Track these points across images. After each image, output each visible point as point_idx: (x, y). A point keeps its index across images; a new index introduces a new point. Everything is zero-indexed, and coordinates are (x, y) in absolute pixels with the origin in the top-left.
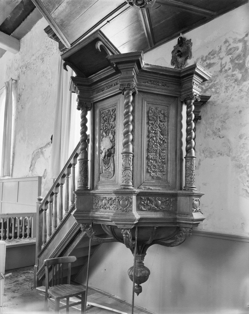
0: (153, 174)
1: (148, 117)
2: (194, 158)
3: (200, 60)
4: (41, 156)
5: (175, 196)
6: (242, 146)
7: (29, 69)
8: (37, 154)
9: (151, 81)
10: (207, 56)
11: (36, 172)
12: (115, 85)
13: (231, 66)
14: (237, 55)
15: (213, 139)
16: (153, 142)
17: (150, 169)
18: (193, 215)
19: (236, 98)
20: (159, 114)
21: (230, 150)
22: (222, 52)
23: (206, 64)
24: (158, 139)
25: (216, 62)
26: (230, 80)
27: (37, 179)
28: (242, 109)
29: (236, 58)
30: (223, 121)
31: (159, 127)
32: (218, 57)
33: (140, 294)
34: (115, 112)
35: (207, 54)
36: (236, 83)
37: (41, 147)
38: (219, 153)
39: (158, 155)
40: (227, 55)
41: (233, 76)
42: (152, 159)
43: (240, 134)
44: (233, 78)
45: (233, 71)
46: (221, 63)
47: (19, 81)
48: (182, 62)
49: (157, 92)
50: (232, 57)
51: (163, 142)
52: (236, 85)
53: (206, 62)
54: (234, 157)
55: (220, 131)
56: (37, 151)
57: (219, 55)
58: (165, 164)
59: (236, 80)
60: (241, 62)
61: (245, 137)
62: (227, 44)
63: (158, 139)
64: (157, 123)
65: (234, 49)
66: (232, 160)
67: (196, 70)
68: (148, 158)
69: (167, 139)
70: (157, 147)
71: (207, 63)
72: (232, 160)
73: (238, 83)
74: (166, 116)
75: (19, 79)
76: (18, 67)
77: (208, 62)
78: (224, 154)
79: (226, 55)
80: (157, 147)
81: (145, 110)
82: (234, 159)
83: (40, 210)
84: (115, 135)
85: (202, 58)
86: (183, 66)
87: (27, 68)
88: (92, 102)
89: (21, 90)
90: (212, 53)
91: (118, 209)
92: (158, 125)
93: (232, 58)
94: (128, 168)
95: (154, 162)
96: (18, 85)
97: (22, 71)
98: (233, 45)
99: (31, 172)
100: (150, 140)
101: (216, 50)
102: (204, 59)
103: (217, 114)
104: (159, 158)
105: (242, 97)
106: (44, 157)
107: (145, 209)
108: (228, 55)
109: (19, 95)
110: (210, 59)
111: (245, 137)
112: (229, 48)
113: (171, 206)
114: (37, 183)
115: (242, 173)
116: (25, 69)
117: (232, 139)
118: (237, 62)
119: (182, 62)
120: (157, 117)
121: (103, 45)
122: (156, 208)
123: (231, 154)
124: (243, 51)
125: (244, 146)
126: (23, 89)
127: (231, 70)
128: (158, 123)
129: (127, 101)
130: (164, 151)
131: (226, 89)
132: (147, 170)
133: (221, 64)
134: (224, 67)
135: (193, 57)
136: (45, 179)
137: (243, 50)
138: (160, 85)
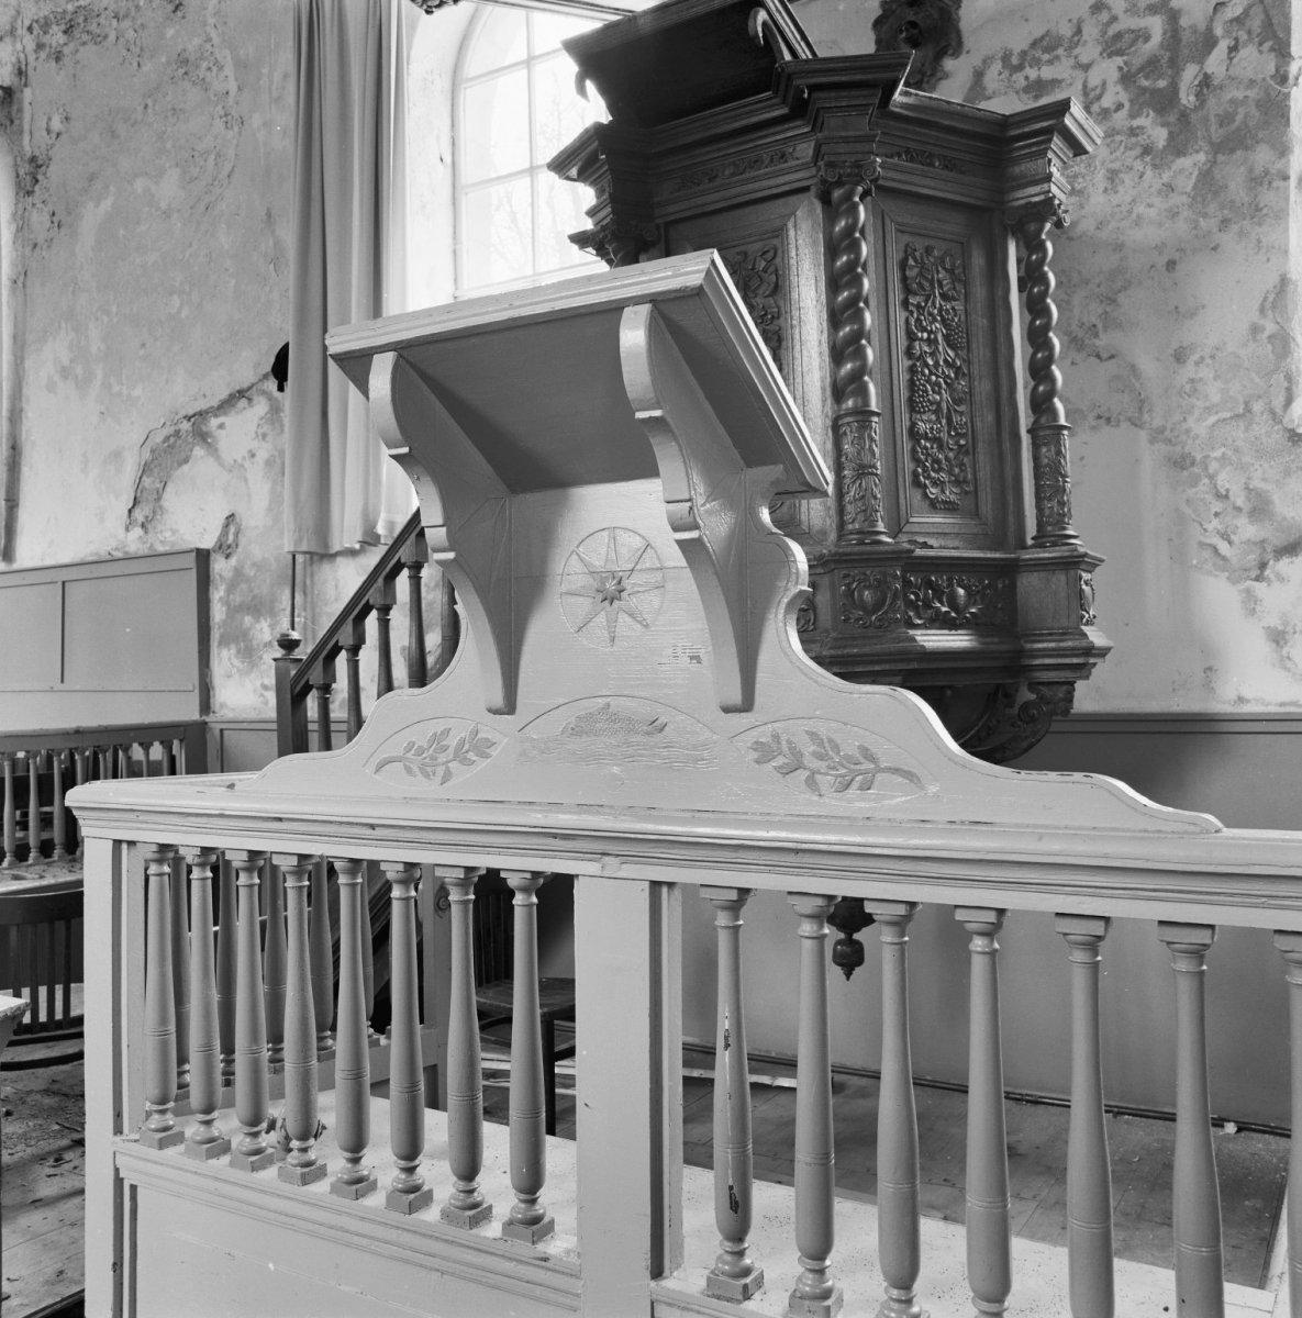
0: (933, 491)
1: (904, 279)
2: (1066, 432)
3: (997, 66)
4: (199, 451)
5: (1010, 570)
6: (1188, 388)
7: (85, 37)
8: (171, 447)
9: (908, 151)
10: (1024, 53)
11: (174, 532)
12: (772, 160)
13: (1124, 97)
14: (1145, 58)
15: (1073, 363)
16: (927, 371)
17: (924, 471)
18: (1086, 635)
19: (1152, 212)
20: (938, 272)
21: (1142, 404)
22: (1086, 41)
23: (1023, 83)
24: (941, 363)
25: (1065, 75)
26: (1122, 149)
27: (191, 561)
28: (1177, 256)
29: (1141, 69)
30: (1109, 298)
31: (941, 316)
32: (1072, 61)
33: (858, 971)
34: (778, 260)
35: (1024, 45)
36: (1148, 159)
37: (191, 412)
38: (1099, 417)
39: (944, 421)
40: (1105, 55)
41: (1133, 132)
42: (927, 439)
43: (1175, 345)
44: (1133, 140)
45: (1133, 116)
46: (1085, 81)
47: (27, 92)
48: (923, 65)
49: (931, 192)
50: (1126, 63)
51: (956, 374)
52: (1149, 168)
53: (1024, 73)
54: (1161, 430)
55: (1096, 335)
56: (169, 430)
57: (1076, 51)
58: (967, 453)
59: (1147, 150)
60: (1162, 84)
61: (1196, 357)
62: (1104, 17)
63: (941, 363)
64: (934, 303)
65: (1132, 36)
66: (1152, 441)
67: (1068, 121)
68: (913, 433)
69: (968, 362)
70: (940, 393)
71: (1027, 78)
72: (1152, 441)
73: (1158, 161)
74: (960, 278)
75: (26, 85)
76: (15, 19)
77: (1033, 73)
78: (1119, 421)
79: (1101, 54)
80: (940, 393)
81: (895, 256)
82: (1157, 435)
83: (298, 688)
84: (779, 347)
85: (1006, 58)
86: (928, 82)
87: (77, 33)
88: (659, 221)
89: (42, 138)
90: (1045, 43)
91: (849, 618)
92: (936, 311)
93: (1126, 69)
94: (871, 467)
95: (932, 448)
96: (20, 110)
97: (40, 46)
98: (1127, 22)
99: (138, 531)
100: (914, 365)
101: (1062, 32)
102: (1015, 61)
103: (1080, 272)
104: (949, 434)
105: (1176, 210)
106: (218, 458)
107: (919, 622)
108: (1110, 56)
109: (33, 159)
110: (1037, 63)
111: (1196, 357)
112: (1111, 32)
113: (1001, 609)
114: (191, 578)
115: (1193, 487)
116: (60, 34)
117: (1148, 365)
118: (1146, 83)
119: (923, 65)
120: (931, 282)
121: (770, 22)
122: (953, 614)
123: (1146, 417)
124: (1169, 45)
125: (1196, 390)
126: (58, 135)
127: (1124, 113)
128: (938, 306)
129: (847, 223)
130: (962, 408)
131: (1111, 180)
132: (915, 475)
133: (1085, 86)
134: (1099, 98)
135: (966, 49)
136: (233, 561)
137: (1165, 43)
138: (937, 164)
